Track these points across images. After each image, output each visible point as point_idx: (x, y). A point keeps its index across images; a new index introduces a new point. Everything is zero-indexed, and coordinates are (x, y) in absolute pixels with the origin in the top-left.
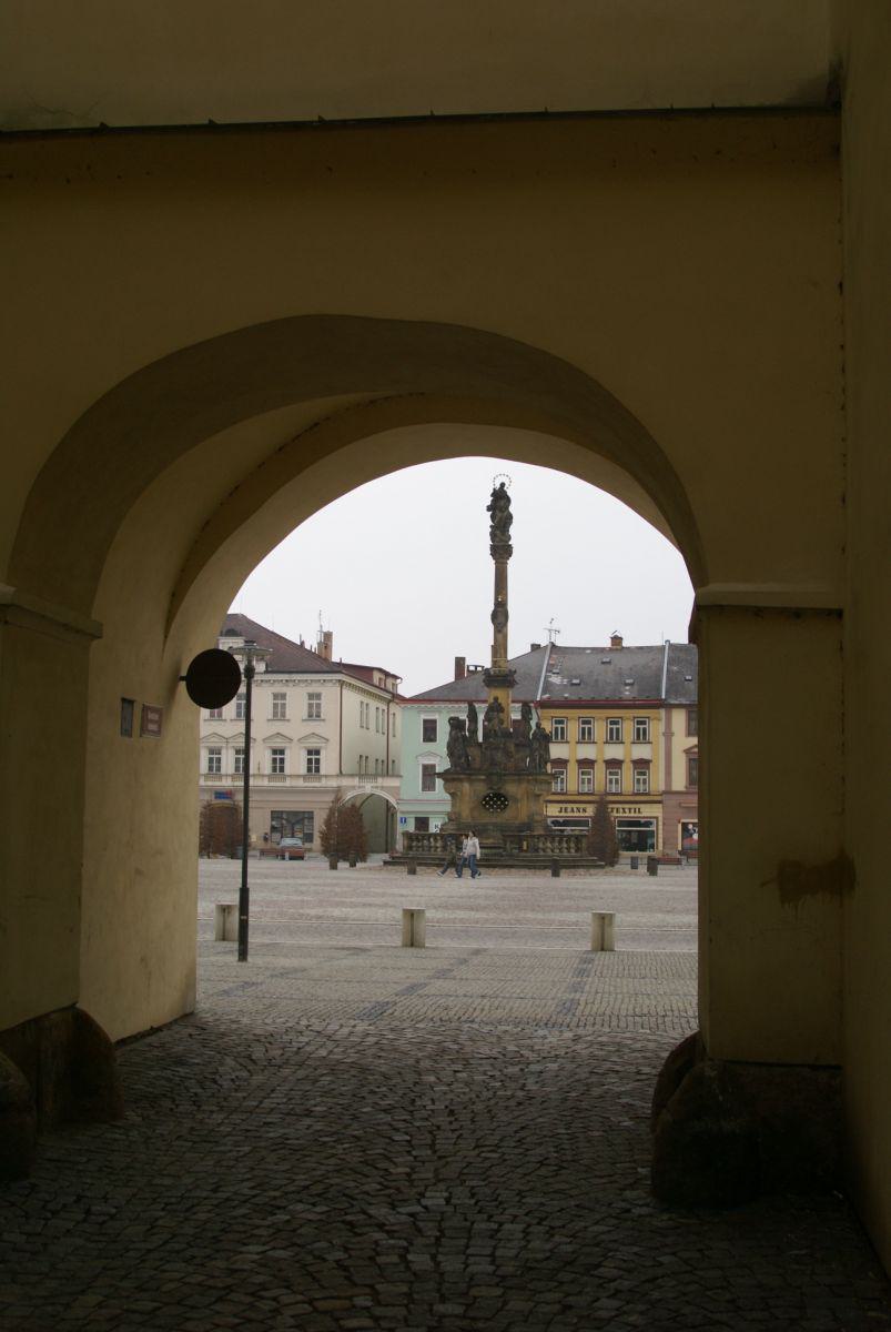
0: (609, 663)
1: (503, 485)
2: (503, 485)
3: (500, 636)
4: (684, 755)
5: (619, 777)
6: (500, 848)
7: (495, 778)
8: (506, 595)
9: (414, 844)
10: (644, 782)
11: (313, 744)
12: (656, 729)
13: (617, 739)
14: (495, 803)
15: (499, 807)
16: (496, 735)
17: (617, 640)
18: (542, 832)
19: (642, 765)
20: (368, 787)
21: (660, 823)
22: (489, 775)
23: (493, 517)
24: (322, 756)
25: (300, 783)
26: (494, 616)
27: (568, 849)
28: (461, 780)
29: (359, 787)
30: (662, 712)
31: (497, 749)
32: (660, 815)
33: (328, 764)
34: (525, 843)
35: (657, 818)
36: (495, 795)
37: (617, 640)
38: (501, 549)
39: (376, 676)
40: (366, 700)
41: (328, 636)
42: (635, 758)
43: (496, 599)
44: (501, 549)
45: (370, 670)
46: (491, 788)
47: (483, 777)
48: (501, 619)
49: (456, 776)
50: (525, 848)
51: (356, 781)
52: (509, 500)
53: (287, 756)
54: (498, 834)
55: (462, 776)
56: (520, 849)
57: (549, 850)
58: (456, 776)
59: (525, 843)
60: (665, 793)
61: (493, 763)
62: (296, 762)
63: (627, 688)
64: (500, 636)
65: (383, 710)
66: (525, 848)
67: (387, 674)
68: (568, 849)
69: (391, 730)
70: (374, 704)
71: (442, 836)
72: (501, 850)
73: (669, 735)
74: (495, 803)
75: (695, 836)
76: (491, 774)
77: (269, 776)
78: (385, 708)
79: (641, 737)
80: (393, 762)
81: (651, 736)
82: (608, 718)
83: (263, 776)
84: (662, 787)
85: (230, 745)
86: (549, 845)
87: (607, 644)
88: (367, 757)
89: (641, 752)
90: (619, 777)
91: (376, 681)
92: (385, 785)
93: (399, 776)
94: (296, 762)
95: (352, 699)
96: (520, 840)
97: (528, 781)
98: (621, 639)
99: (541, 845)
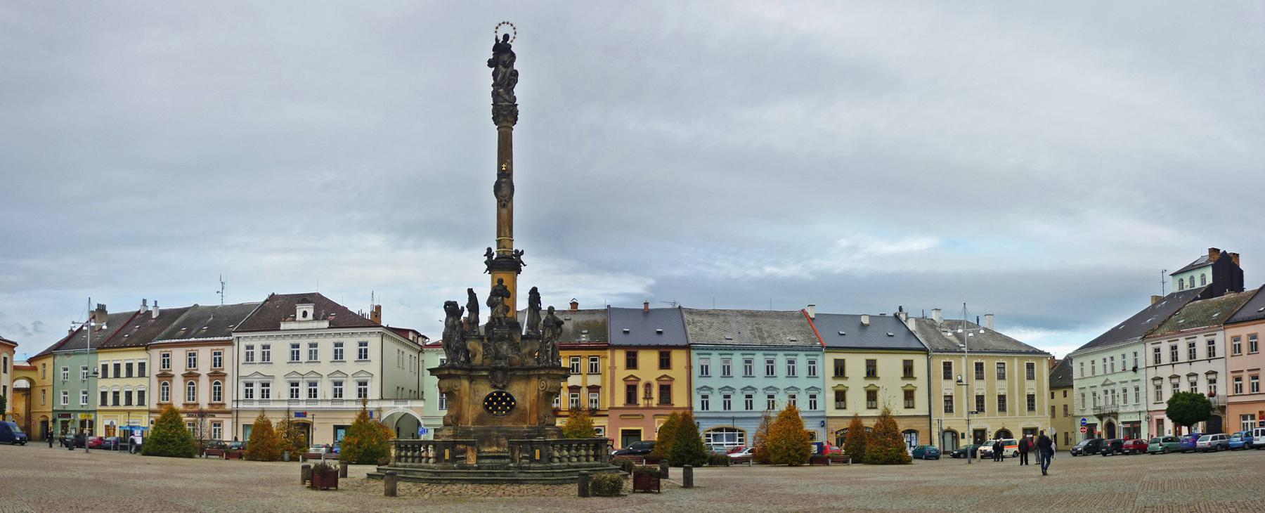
0: (570, 320)
1: (506, 37)
2: (506, 37)
3: (504, 211)
4: (623, 382)
5: (578, 398)
6: (507, 457)
7: (499, 375)
8: (511, 163)
9: (403, 453)
10: (596, 402)
11: (363, 378)
12: (604, 364)
13: (577, 371)
14: (499, 403)
15: (504, 408)
16: (500, 324)
17: (574, 305)
18: (555, 438)
19: (594, 389)
20: (402, 408)
21: (606, 430)
22: (493, 370)
23: (495, 75)
24: (368, 387)
25: (328, 405)
26: (497, 188)
27: (587, 456)
28: (458, 377)
29: (395, 408)
30: (609, 353)
31: (502, 339)
32: (606, 424)
33: (373, 391)
34: (537, 452)
35: (604, 426)
36: (499, 394)
37: (574, 305)
38: (505, 113)
39: (411, 336)
40: (402, 349)
41: (378, 308)
42: (589, 385)
43: (500, 167)
44: (505, 113)
45: (408, 331)
46: (495, 387)
47: (485, 373)
48: (505, 191)
49: (453, 372)
50: (537, 457)
51: (392, 404)
52: (513, 56)
53: (344, 387)
54: (504, 441)
55: (459, 372)
56: (532, 459)
57: (565, 459)
58: (453, 372)
59: (537, 452)
60: (610, 408)
61: (497, 356)
62: (350, 391)
63: (584, 336)
64: (504, 211)
65: (415, 357)
66: (537, 457)
67: (418, 335)
68: (587, 456)
69: (421, 371)
70: (408, 352)
71: (434, 444)
72: (507, 460)
73: (613, 368)
74: (499, 403)
75: (905, 441)
76: (496, 369)
77: (332, 401)
78: (417, 356)
79: (594, 370)
80: (423, 392)
81: (600, 369)
82: (570, 357)
83: (328, 400)
84: (608, 405)
85: (305, 379)
86: (566, 453)
87: (568, 307)
88: (403, 389)
89: (594, 380)
90: (578, 398)
91: (411, 338)
92: (412, 406)
93: (424, 400)
94: (350, 391)
95: (392, 347)
96: (533, 446)
97: (539, 377)
98: (577, 304)
99: (556, 454)
